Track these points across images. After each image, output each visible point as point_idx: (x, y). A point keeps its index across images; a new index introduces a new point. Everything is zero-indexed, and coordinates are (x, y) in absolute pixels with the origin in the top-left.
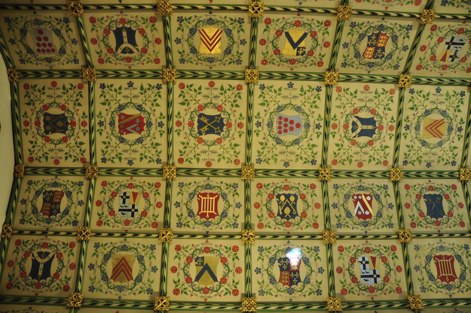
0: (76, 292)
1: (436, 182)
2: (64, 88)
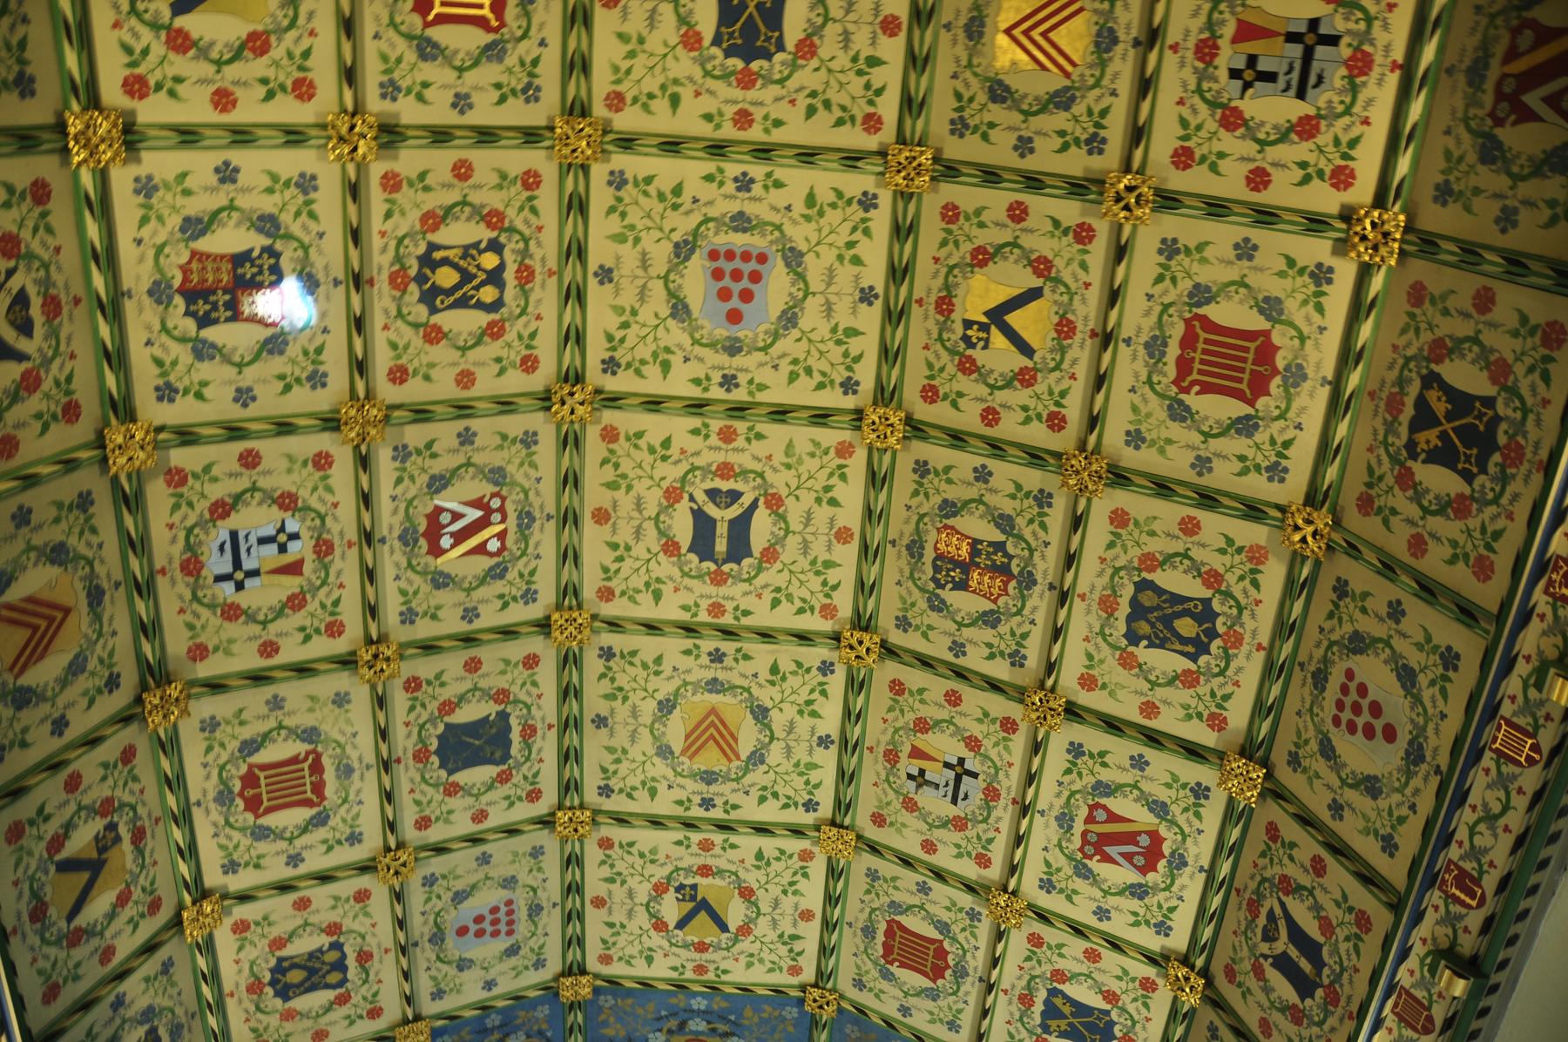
1: (547, 746)
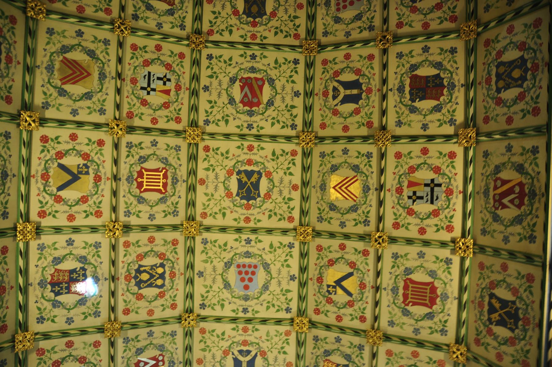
0: (47, 11)
2: (296, 17)
